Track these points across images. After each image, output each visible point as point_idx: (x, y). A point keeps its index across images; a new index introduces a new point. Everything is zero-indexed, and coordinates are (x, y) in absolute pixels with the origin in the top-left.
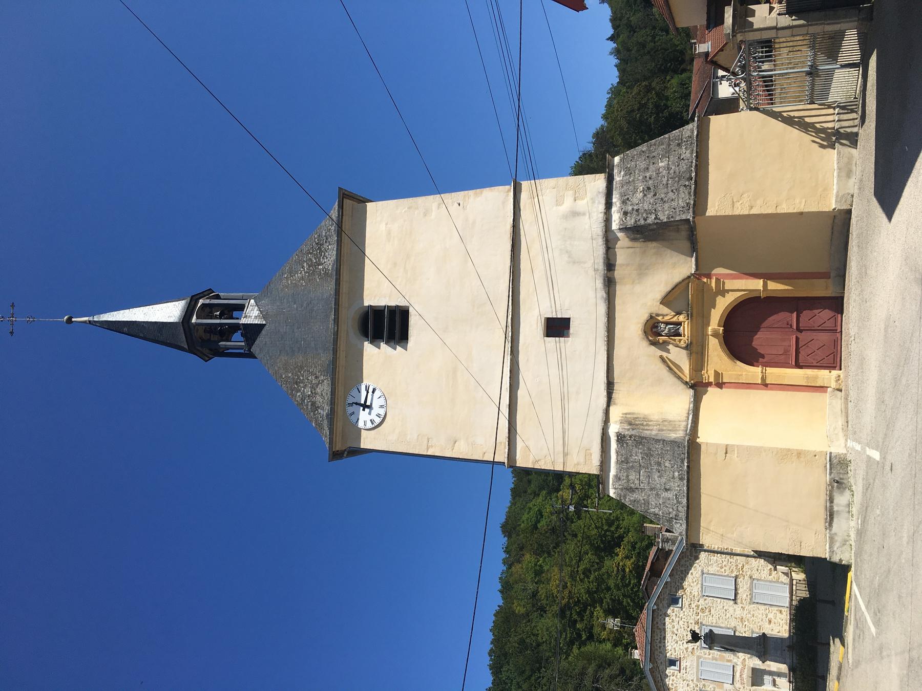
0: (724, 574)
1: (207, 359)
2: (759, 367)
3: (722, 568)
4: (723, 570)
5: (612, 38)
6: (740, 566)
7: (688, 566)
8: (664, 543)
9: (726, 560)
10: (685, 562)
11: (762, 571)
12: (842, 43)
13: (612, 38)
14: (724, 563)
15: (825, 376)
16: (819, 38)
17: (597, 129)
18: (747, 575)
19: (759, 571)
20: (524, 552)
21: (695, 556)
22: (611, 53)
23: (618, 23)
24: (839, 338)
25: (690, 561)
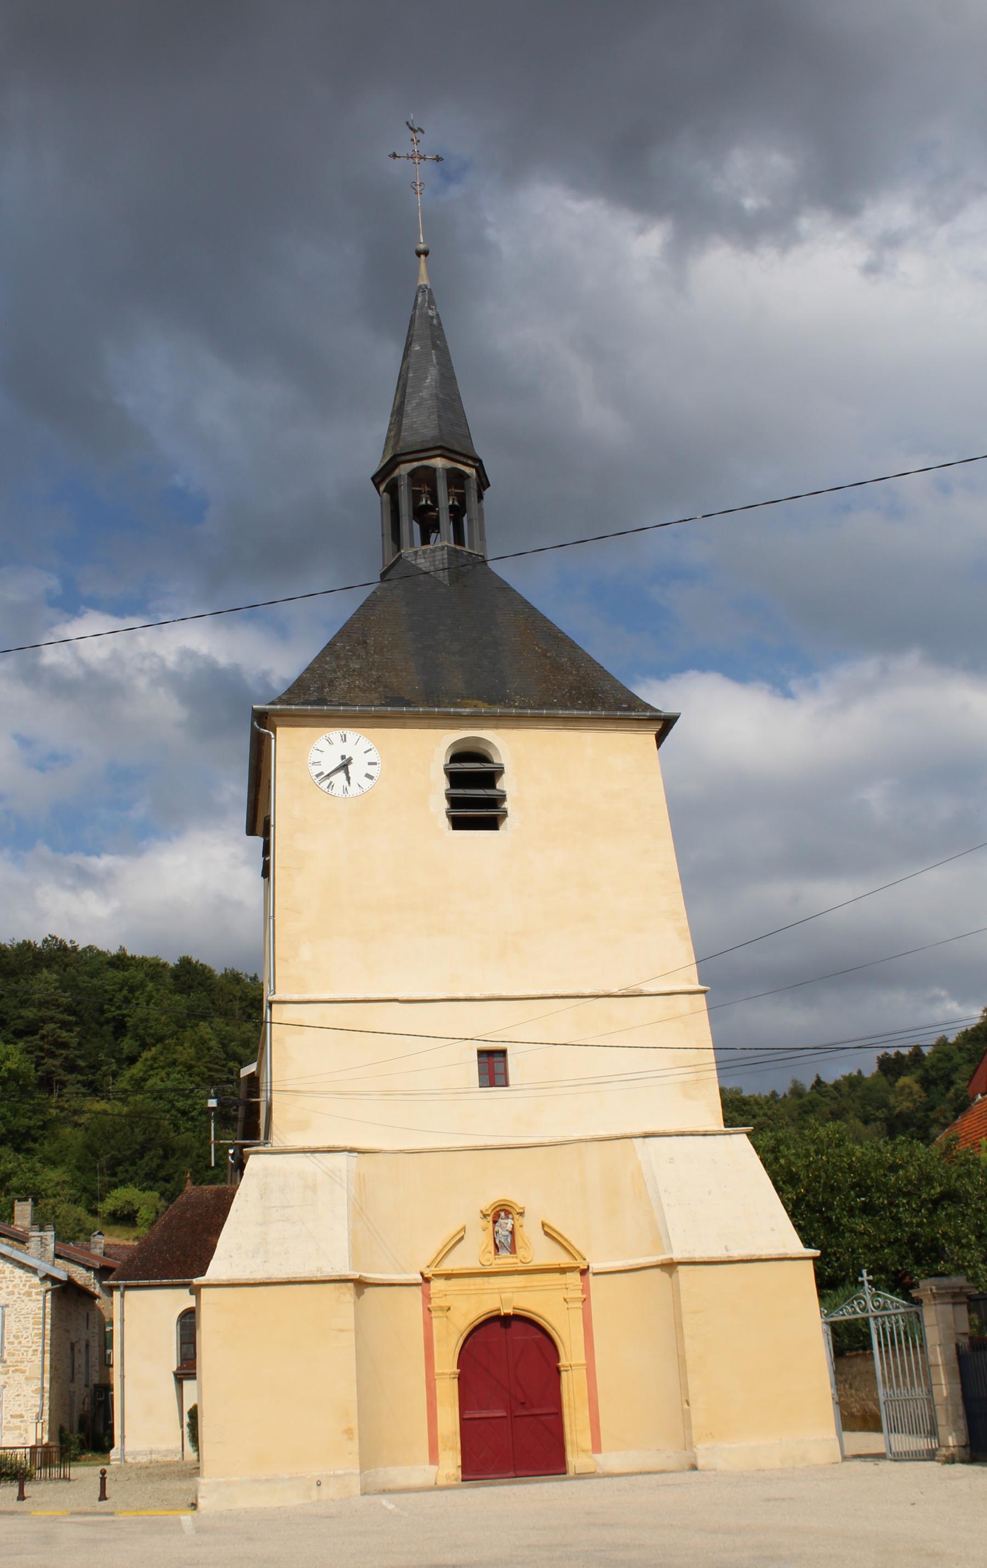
0: (6, 1342)
1: (377, 480)
2: (458, 1368)
3: (16, 1337)
4: (12, 1339)
5: (819, 1082)
6: (21, 1367)
7: (12, 1281)
8: (39, 1239)
9: (30, 1344)
10: (20, 1277)
11: (18, 1402)
12: (934, 1439)
13: (819, 1082)
14: (24, 1341)
15: (451, 1461)
16: (917, 1403)
17: (226, 970)
18: (9, 1378)
19: (17, 1398)
20: (779, 1160)
21: (31, 1293)
22: (795, 1082)
23: (845, 1089)
24: (508, 1475)
25: (21, 1284)
